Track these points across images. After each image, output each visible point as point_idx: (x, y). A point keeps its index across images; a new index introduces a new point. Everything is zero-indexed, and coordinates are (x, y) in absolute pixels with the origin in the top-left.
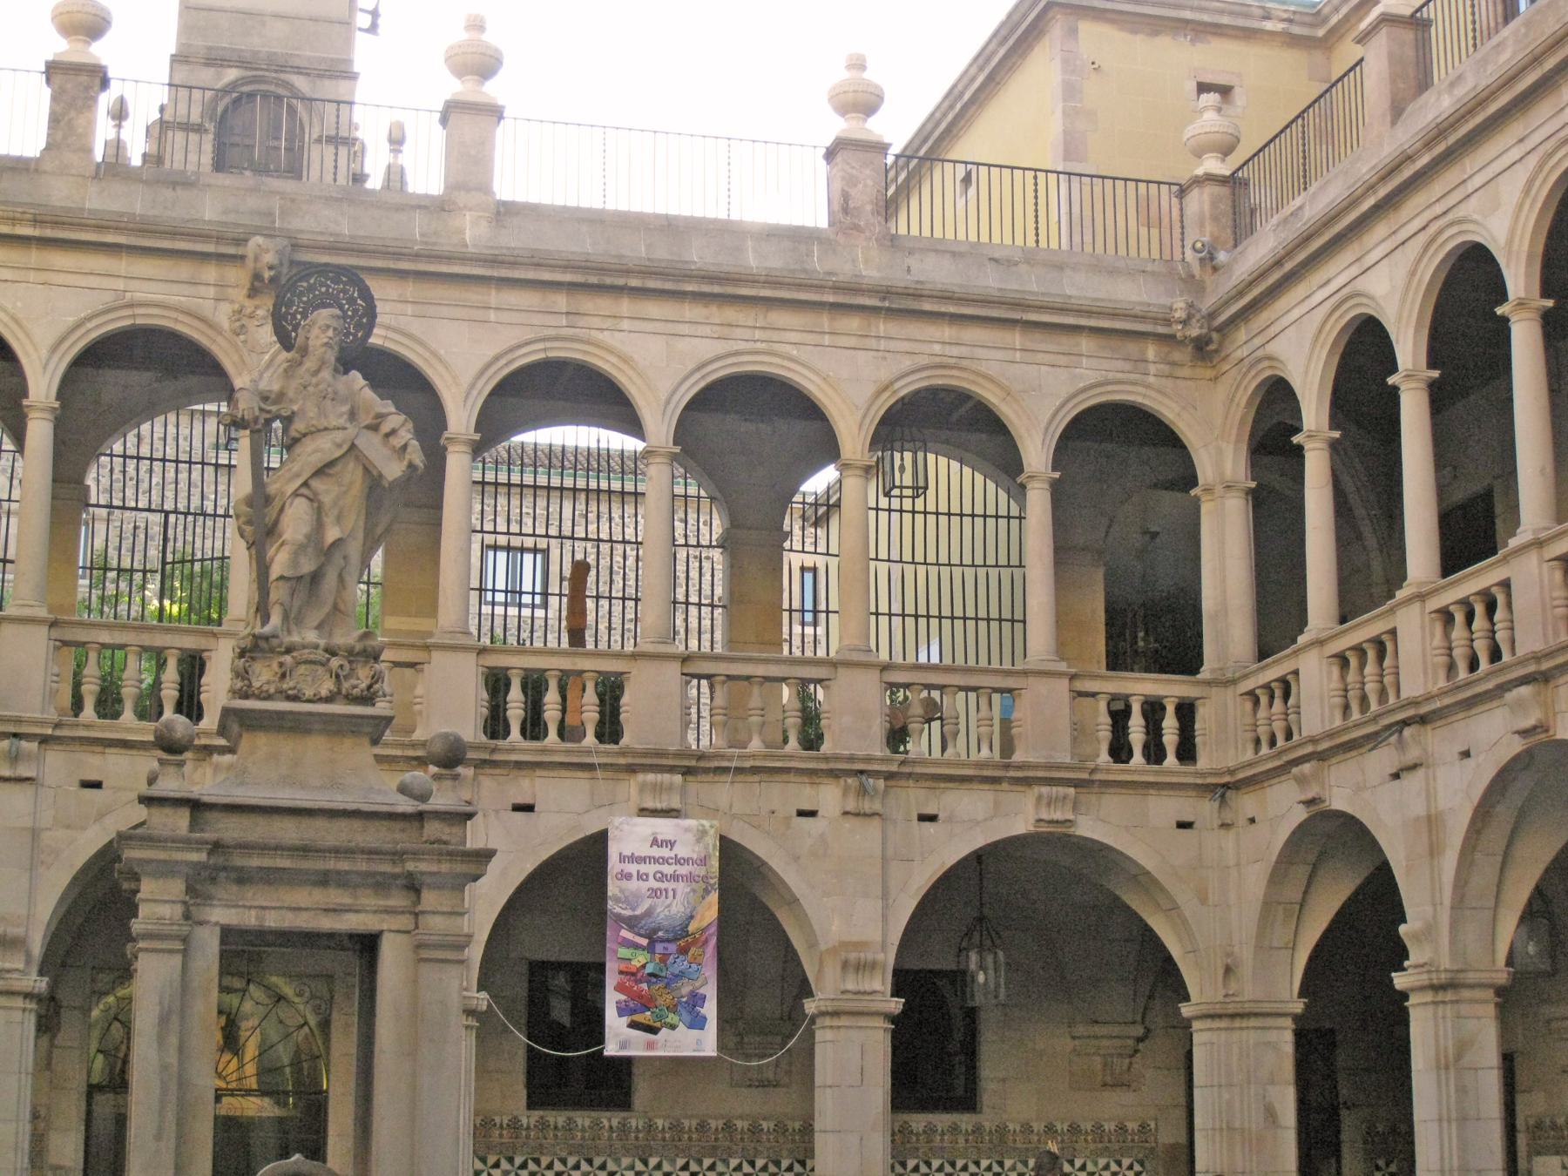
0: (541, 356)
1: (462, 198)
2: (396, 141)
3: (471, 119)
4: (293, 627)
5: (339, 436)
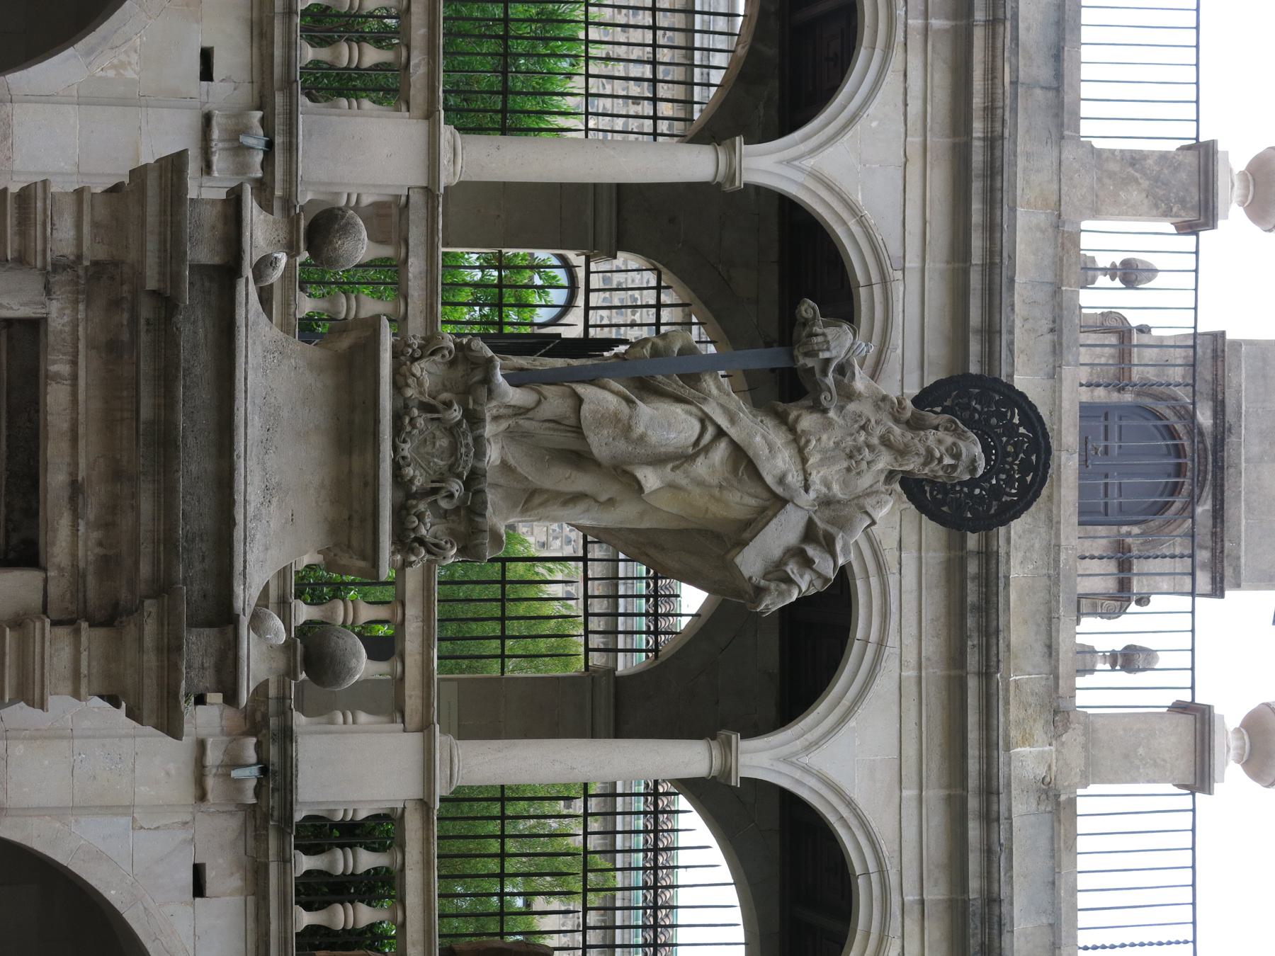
0: (858, 868)
1: (1073, 737)
2: (1129, 659)
3: (1191, 746)
4: (504, 425)
5: (794, 479)
